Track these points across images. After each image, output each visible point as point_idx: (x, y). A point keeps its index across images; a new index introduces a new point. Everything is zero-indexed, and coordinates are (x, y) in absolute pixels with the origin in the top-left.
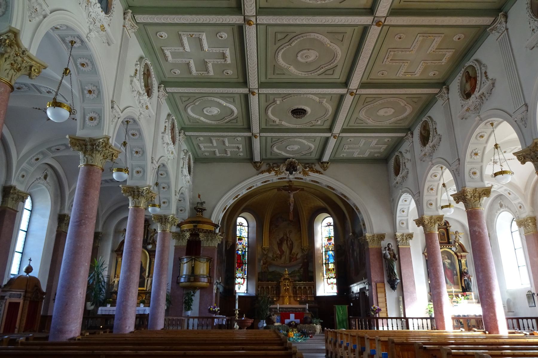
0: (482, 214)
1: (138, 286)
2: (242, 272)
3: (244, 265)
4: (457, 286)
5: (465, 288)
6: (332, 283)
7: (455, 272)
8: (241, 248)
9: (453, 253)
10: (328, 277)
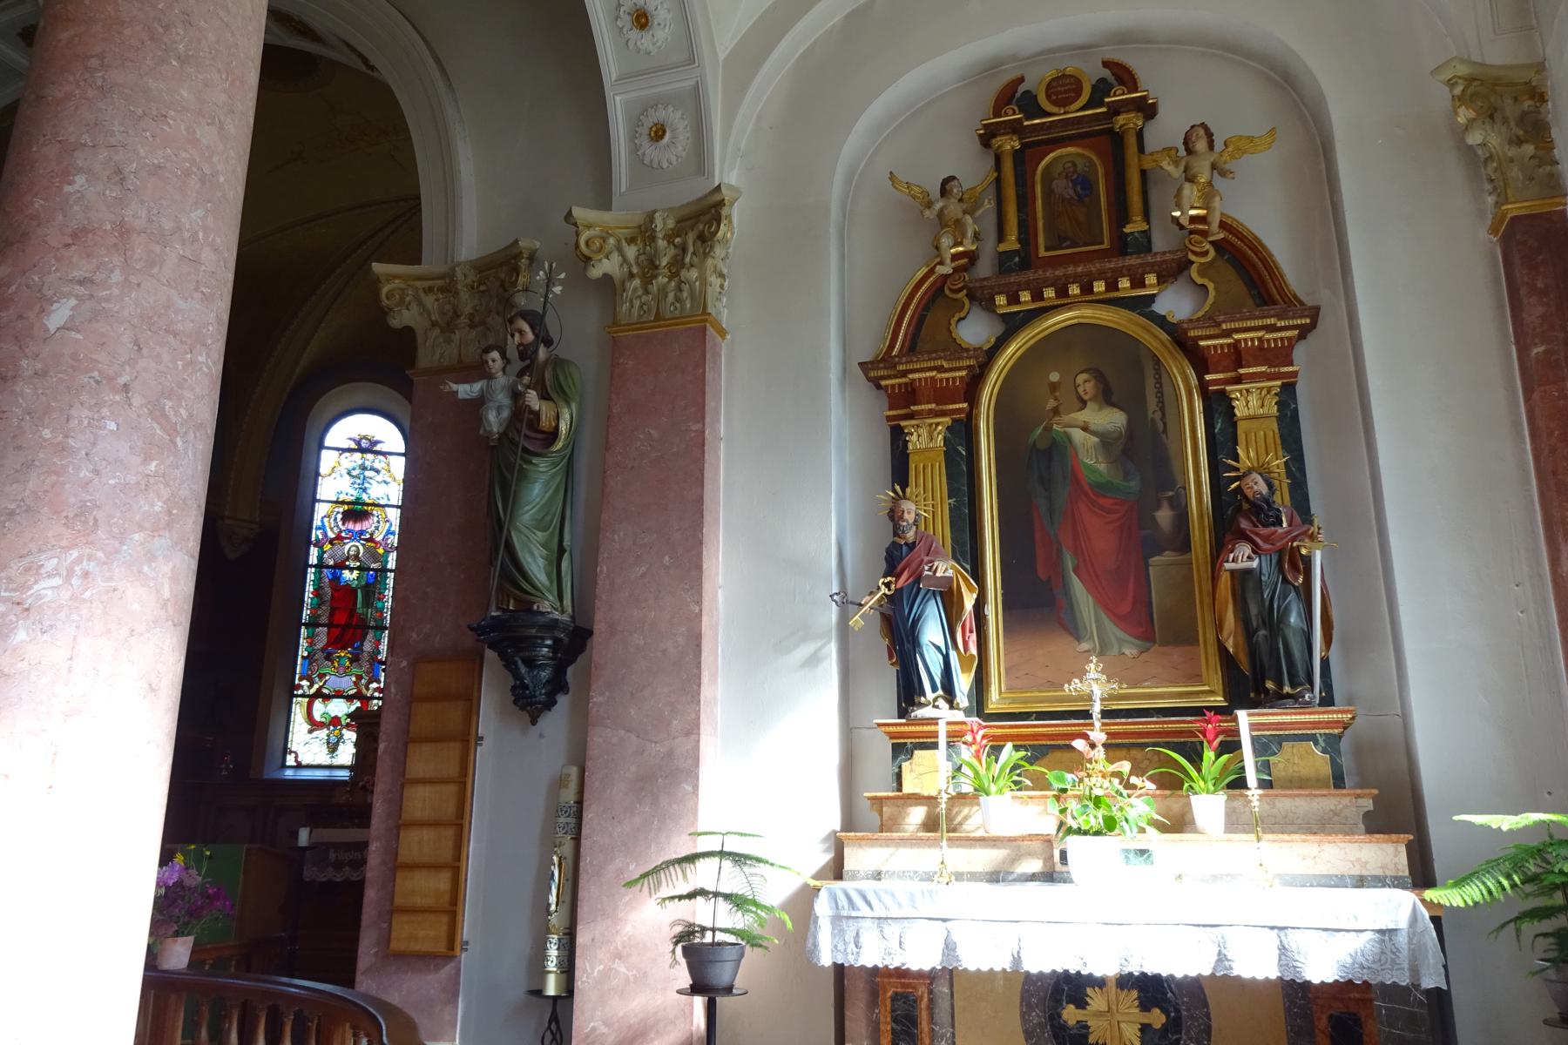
2: (355, 670)
3: (370, 636)
4: (1176, 654)
6: (335, 721)
7: (1164, 516)
8: (356, 557)
9: (1155, 340)
10: (319, 690)
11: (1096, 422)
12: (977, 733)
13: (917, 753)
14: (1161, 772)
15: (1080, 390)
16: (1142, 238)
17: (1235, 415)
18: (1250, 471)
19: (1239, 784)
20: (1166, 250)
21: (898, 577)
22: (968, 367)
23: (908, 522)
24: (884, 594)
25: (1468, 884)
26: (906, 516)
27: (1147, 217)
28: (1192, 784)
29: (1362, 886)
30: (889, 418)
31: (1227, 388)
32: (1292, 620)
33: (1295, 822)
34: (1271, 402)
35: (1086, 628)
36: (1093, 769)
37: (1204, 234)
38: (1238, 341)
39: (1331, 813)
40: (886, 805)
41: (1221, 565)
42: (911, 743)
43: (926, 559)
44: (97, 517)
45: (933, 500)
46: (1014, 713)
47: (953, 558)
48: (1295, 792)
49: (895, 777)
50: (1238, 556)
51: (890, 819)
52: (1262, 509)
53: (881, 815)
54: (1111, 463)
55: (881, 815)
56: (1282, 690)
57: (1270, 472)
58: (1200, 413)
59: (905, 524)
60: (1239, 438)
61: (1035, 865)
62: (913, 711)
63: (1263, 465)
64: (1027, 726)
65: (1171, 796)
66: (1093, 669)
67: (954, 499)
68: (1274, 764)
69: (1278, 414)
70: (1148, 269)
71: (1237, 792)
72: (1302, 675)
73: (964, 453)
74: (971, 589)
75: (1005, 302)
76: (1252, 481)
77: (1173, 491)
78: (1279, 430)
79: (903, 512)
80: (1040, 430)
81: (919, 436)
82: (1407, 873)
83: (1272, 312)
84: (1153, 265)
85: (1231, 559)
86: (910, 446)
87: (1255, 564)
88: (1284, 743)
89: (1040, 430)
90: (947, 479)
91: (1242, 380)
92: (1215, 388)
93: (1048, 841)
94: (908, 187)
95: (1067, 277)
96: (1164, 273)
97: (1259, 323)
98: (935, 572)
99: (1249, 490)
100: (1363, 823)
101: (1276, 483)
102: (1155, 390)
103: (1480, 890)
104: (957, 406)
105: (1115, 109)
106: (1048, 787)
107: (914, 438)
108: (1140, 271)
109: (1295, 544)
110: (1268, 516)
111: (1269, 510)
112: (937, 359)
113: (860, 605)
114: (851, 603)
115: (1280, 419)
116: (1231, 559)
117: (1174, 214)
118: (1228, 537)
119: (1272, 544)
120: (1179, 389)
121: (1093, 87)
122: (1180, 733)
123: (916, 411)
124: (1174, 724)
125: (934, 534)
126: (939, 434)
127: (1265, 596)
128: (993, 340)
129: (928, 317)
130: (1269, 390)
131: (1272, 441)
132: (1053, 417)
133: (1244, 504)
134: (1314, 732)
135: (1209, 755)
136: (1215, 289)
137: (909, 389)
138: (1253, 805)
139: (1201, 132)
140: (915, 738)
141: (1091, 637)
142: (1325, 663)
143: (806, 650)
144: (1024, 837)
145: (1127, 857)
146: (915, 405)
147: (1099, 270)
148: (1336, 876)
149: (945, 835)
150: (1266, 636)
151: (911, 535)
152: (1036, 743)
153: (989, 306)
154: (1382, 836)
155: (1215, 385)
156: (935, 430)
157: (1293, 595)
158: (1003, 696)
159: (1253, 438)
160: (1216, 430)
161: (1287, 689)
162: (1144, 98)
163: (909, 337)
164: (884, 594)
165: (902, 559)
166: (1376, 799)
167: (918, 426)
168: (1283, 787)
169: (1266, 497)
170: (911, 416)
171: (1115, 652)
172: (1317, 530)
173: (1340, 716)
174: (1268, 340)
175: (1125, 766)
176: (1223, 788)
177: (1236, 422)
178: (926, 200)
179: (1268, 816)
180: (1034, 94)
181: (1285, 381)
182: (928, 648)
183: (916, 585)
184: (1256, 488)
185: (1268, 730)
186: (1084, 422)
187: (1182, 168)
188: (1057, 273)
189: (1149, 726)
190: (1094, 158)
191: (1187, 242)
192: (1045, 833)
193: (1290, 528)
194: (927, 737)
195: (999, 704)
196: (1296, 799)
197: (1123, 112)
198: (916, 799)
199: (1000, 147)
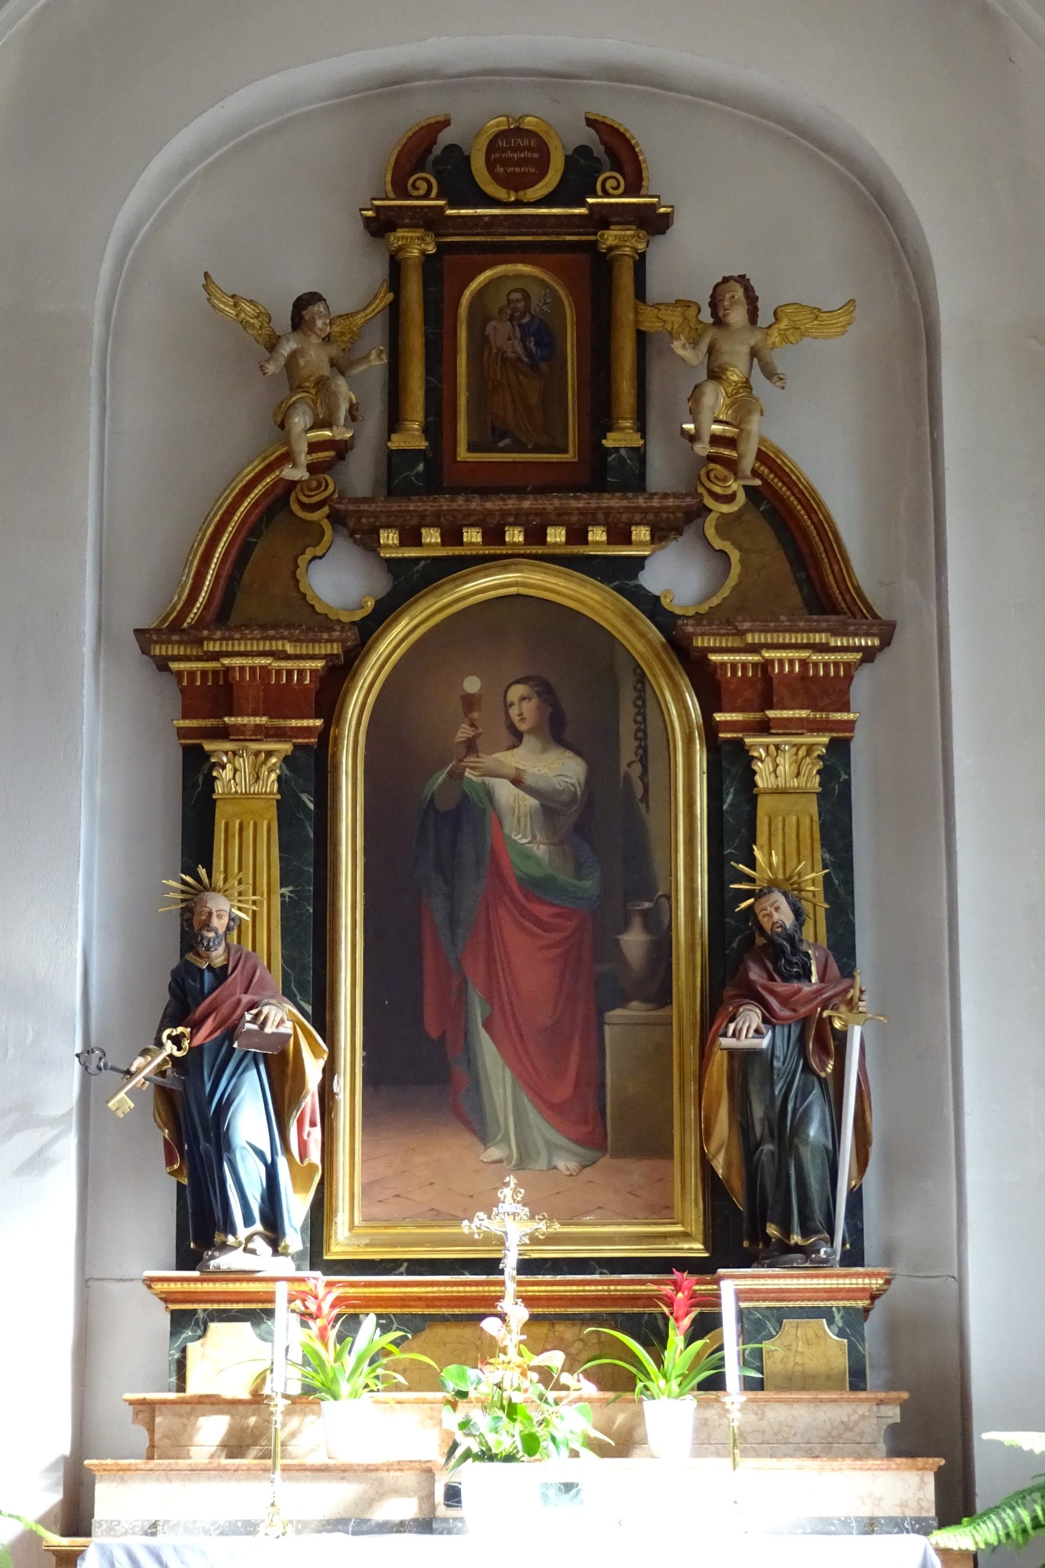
0: (699, 413)
1: (177, 738)
4: (637, 1170)
5: (739, 1199)
11: (535, 770)
12: (323, 1299)
13: (214, 1327)
14: (600, 1366)
15: (514, 712)
16: (631, 459)
17: (755, 785)
18: (773, 885)
19: (715, 1383)
20: (669, 492)
21: (196, 1026)
22: (325, 657)
23: (216, 933)
24: (171, 1056)
25: (984, 1522)
26: (215, 922)
27: (641, 428)
28: (649, 1384)
29: (872, 1532)
30: (182, 733)
31: (748, 740)
32: (812, 1132)
33: (791, 1440)
34: (811, 770)
35: (498, 1122)
36: (509, 1363)
37: (732, 465)
38: (769, 662)
39: (842, 1426)
40: (161, 1413)
41: (714, 1041)
42: (205, 1310)
43: (246, 999)
44: (517, 1364)
45: (254, 894)
46: (373, 1261)
47: (284, 994)
48: (795, 1395)
49: (174, 1368)
50: (741, 1029)
51: (166, 1436)
52: (783, 951)
53: (151, 1430)
54: (554, 844)
55: (151, 1430)
56: (789, 1238)
57: (800, 890)
58: (702, 773)
59: (212, 935)
60: (758, 822)
61: (408, 1509)
62: (213, 1257)
63: (791, 877)
64: (394, 1284)
65: (614, 1400)
66: (510, 1198)
67: (290, 888)
68: (768, 1352)
69: (820, 790)
70: (638, 517)
71: (712, 1395)
72: (819, 1216)
73: (311, 806)
74: (316, 1053)
75: (396, 542)
76: (772, 905)
77: (650, 900)
78: (820, 813)
79: (210, 914)
80: (441, 777)
81: (235, 770)
82: (932, 1513)
83: (824, 625)
84: (645, 511)
85: (730, 1032)
86: (219, 787)
87: (764, 1043)
88: (785, 1321)
89: (441, 777)
90: (281, 850)
91: (770, 728)
92: (729, 735)
93: (428, 1472)
94: (235, 305)
95: (505, 513)
96: (663, 525)
97: (803, 638)
98: (263, 1025)
99: (766, 919)
100: (885, 1442)
101: (807, 907)
102: (635, 727)
103: (997, 1529)
104: (305, 723)
105: (602, 218)
106: (441, 1387)
107: (227, 773)
108: (624, 518)
109: (825, 1014)
110: (789, 962)
111: (794, 954)
112: (277, 639)
113: (128, 1072)
114: (113, 1069)
115: (822, 797)
116: (730, 1032)
117: (685, 426)
118: (729, 992)
119: (794, 1010)
120: (675, 746)
121: (568, 159)
122: (633, 1299)
123: (234, 726)
124: (626, 1284)
125: (254, 949)
126: (270, 771)
127: (776, 1092)
128: (370, 604)
129: (258, 548)
130: (810, 748)
131: (808, 836)
132: (465, 756)
133: (757, 936)
134: (828, 1304)
135: (676, 1339)
136: (742, 561)
137: (221, 683)
138: (731, 1416)
139: (740, 293)
140: (212, 1302)
141: (506, 1139)
142: (856, 1197)
143: (28, 1141)
144: (392, 1465)
145: (545, 1496)
146: (230, 715)
147: (556, 509)
148: (839, 1519)
149: (280, 1462)
150: (772, 1153)
151: (218, 956)
152: (406, 1311)
153: (368, 540)
154: (904, 1460)
155: (731, 731)
156: (264, 763)
157: (816, 1091)
158: (356, 1231)
159: (780, 825)
160: (725, 807)
161: (796, 1239)
162: (653, 207)
163: (222, 582)
164: (171, 1056)
165: (205, 997)
166: (904, 1406)
167: (234, 753)
168: (779, 1388)
169: (790, 932)
170: (223, 733)
171: (542, 1164)
172: (858, 993)
173: (867, 1281)
174: (816, 665)
175: (555, 1359)
176: (692, 1390)
177: (756, 797)
178: (264, 332)
179: (754, 1431)
180: (466, 154)
181: (835, 735)
182: (245, 1152)
183: (227, 1043)
184: (776, 916)
185: (765, 1300)
186: (517, 769)
187: (704, 347)
188: (489, 505)
189: (587, 1288)
190: (562, 292)
191: (703, 473)
192: (424, 1459)
193: (822, 985)
194: (232, 1302)
195: (348, 1245)
196: (795, 1405)
197: (618, 223)
198: (212, 1404)
199: (401, 249)
